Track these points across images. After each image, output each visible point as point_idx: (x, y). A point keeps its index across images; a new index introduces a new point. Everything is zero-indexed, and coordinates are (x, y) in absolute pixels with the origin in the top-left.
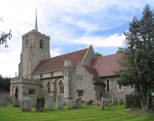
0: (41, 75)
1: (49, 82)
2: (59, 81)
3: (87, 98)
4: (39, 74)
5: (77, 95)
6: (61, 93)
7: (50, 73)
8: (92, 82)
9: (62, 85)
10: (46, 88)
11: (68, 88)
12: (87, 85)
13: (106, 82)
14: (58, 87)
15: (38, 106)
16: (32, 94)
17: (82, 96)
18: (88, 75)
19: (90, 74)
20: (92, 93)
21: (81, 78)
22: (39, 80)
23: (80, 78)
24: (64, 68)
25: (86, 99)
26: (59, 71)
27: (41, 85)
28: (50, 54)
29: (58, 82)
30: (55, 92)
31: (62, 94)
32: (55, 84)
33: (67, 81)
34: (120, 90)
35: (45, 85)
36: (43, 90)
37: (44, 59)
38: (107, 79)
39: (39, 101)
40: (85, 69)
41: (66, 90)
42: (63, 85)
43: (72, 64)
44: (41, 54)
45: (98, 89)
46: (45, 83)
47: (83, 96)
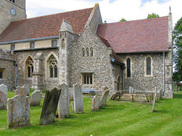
0: (13, 45)
1: (30, 57)
2: (49, 55)
3: (100, 87)
4: (9, 44)
5: (82, 81)
6: (52, 76)
7: (29, 41)
8: (109, 60)
9: (53, 64)
10: (24, 67)
11: (66, 69)
12: (99, 64)
13: (125, 62)
14: (47, 66)
15: (47, 111)
16: (88, 83)
17: (90, 83)
18: (102, 48)
19: (106, 47)
20: (108, 79)
21: (90, 52)
22: (12, 53)
23: (87, 53)
24: (60, 34)
25: (98, 89)
26: (40, 40)
27: (14, 62)
28: (25, 12)
29: (47, 58)
30: (41, 75)
31: (54, 79)
32: (42, 60)
33: (66, 56)
34: (149, 76)
35: (22, 62)
36: (19, 71)
37: (17, 20)
38: (127, 57)
39: (50, 99)
40: (96, 39)
41: (63, 71)
42: (55, 63)
43: (73, 28)
44: (12, 11)
45: (116, 73)
46: (22, 59)
47: (91, 83)
